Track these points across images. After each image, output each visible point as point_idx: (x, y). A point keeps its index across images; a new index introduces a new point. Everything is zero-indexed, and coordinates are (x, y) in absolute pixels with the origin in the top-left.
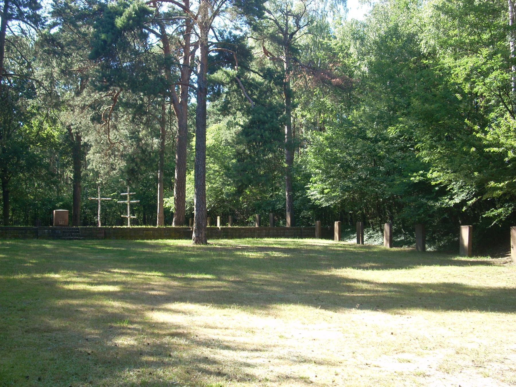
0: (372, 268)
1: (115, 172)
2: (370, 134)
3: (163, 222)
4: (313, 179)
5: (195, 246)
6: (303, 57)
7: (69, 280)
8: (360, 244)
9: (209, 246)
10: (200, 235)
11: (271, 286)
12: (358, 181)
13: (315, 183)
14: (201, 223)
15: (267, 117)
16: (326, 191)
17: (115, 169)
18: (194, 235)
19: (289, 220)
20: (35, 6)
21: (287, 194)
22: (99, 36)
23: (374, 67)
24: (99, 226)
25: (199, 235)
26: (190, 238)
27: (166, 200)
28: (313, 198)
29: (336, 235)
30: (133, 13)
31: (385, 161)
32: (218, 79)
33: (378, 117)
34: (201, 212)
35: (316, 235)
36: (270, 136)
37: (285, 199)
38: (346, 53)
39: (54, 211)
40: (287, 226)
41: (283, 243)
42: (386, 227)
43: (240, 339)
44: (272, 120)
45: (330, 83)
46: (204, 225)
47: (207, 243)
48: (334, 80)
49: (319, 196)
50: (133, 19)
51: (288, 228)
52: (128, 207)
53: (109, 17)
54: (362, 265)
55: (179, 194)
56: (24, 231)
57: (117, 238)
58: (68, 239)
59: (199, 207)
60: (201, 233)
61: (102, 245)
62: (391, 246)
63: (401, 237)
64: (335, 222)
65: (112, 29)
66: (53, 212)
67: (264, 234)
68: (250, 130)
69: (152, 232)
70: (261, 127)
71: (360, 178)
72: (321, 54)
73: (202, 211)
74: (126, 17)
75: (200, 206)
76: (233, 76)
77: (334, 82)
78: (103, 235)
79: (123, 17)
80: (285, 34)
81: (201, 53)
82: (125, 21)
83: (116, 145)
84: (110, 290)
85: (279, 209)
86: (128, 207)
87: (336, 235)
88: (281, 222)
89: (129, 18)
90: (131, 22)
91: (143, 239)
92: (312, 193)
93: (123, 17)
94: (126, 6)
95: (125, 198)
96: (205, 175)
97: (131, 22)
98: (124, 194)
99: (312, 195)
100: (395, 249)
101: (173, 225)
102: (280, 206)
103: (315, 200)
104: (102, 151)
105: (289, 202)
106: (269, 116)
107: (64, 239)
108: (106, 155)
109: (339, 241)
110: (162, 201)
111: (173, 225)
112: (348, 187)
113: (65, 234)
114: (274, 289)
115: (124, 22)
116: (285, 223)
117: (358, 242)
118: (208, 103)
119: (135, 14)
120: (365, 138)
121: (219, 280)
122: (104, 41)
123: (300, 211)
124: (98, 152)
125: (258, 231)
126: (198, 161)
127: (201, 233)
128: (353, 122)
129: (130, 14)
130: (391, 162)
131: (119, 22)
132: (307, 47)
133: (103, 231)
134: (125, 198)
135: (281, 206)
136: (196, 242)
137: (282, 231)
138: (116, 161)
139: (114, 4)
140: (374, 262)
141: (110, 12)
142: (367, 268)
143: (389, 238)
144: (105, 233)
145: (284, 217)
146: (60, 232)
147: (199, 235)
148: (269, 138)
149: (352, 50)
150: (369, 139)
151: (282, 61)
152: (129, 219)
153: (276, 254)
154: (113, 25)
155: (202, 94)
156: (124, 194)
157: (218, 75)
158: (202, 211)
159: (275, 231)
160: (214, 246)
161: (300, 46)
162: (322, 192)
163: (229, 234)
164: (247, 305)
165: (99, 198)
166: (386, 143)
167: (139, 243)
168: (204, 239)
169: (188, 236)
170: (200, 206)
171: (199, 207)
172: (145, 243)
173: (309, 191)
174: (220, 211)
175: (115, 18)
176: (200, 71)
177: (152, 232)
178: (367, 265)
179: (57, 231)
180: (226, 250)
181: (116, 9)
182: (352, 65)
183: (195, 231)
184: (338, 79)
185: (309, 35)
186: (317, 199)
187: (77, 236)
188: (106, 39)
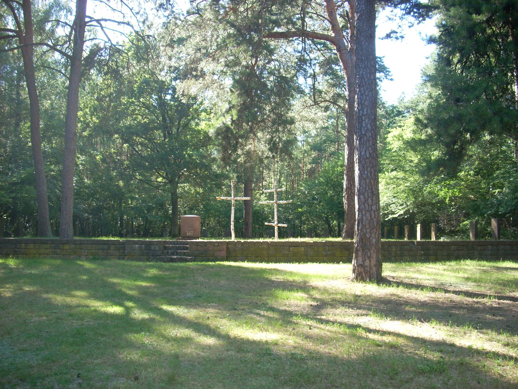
10: (367, 263)
11: (320, 39)
14: (368, 236)
25: (364, 261)
34: (368, 215)
46: (374, 240)
47: (381, 280)
56: (105, 247)
59: (364, 204)
60: (369, 258)
67: (489, 252)
69: (303, 249)
73: (370, 212)
84: (250, 338)
96: (495, 307)
113: (165, 251)
125: (479, 248)
126: (360, 108)
127: (369, 258)
133: (225, 246)
146: (157, 248)
147: (364, 261)
152: (276, 228)
158: (370, 212)
163: (431, 252)
165: (233, 197)
170: (366, 200)
171: (364, 204)
174: (422, 217)
177: (303, 249)
179: (153, 247)
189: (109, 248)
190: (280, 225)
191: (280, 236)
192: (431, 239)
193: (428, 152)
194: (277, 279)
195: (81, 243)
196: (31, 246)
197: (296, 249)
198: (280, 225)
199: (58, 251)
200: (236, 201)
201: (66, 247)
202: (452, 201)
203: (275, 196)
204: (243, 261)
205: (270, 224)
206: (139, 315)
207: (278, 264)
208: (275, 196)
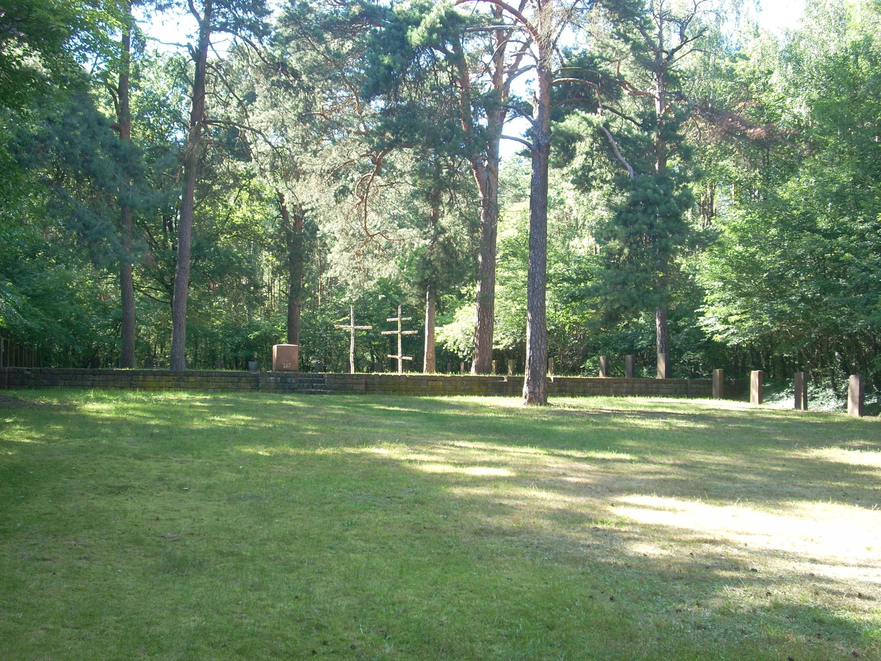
0: (862, 448)
1: (371, 283)
2: (822, 223)
3: (434, 367)
4: (709, 298)
5: (529, 407)
6: (694, 89)
7: (480, 453)
8: (800, 408)
9: (552, 408)
10: (537, 390)
12: (800, 301)
13: (712, 305)
15: (659, 193)
16: (732, 319)
17: (371, 279)
18: (525, 389)
19: (662, 367)
20: (258, 5)
21: (658, 322)
22: (378, 59)
23: (820, 109)
24: (352, 372)
25: (534, 389)
26: (519, 393)
27: (437, 329)
28: (710, 329)
29: (754, 393)
30: (438, 20)
31: (852, 269)
32: (574, 131)
33: (837, 194)
35: (714, 393)
36: (665, 226)
37: (655, 332)
38: (764, 84)
39: (275, 347)
40: (659, 377)
41: (669, 405)
42: (853, 382)
43: (798, 549)
44: (666, 199)
45: (744, 136)
48: (752, 131)
49: (721, 327)
50: (438, 31)
51: (659, 381)
52: (399, 341)
53: (395, 28)
54: (849, 443)
55: (484, 320)
56: (236, 379)
57: (385, 392)
58: (307, 393)
61: (381, 403)
62: (862, 413)
63: (871, 398)
64: (753, 372)
65: (402, 47)
66: (271, 351)
67: (625, 390)
68: (630, 215)
70: (650, 211)
71: (804, 298)
72: (720, 85)
74: (426, 28)
75: (537, 341)
76: (598, 125)
77: (751, 134)
78: (362, 387)
79: (420, 28)
80: (659, 51)
81: (540, 86)
82: (426, 34)
83: (376, 238)
85: (642, 348)
86: (399, 341)
87: (754, 393)
88: (645, 370)
89: (431, 30)
90: (435, 36)
91: (435, 395)
92: (706, 323)
93: (422, 28)
94: (423, 9)
95: (393, 326)
97: (435, 36)
98: (393, 319)
99: (706, 326)
100: (867, 419)
101: (473, 373)
102: (642, 343)
103: (713, 333)
104: (353, 248)
105: (662, 336)
106: (662, 192)
107: (301, 393)
108: (358, 255)
109: (760, 402)
110: (431, 331)
111: (473, 373)
112: (783, 313)
114: (751, 477)
115: (423, 37)
116: (653, 371)
117: (797, 405)
118: (551, 171)
119: (440, 23)
120: (814, 230)
121: (645, 461)
122: (389, 68)
123: (680, 352)
124: (347, 250)
125: (614, 385)
127: (539, 386)
128: (792, 203)
129: (434, 23)
130: (863, 271)
131: (415, 36)
132: (692, 75)
133: (363, 380)
134: (393, 326)
135: (644, 343)
136: (530, 401)
137: (654, 386)
138: (374, 264)
139: (406, 6)
140: (865, 439)
141: (397, 20)
142: (855, 448)
143: (857, 400)
144: (366, 384)
145: (654, 363)
146: (294, 381)
147: (534, 389)
148: (663, 230)
149: (774, 79)
150: (819, 231)
151: (654, 97)
153: (682, 424)
154: (404, 42)
155: (542, 156)
156: (393, 319)
157: (573, 123)
159: (644, 385)
160: (562, 408)
161: (680, 71)
162: (725, 321)
164: (743, 500)
166: (852, 238)
167: (426, 400)
168: (542, 396)
169: (513, 389)
170: (537, 341)
172: (433, 401)
173: (701, 318)
175: (407, 29)
176: (539, 117)
178: (855, 443)
179: (289, 380)
180: (582, 414)
181: (406, 14)
182: (773, 103)
183: (528, 383)
184: (759, 129)
185: (697, 53)
186: (718, 332)
187: (321, 387)
188: (392, 64)
189: (239, 381)
190: (404, 358)
191: (404, 369)
192: (422, 371)
193: (202, 208)
194: (627, 406)
195: (209, 375)
196: (151, 378)
197: (434, 383)
198: (404, 358)
199: (182, 384)
200: (356, 330)
201: (192, 379)
202: (573, 329)
203: (399, 326)
204: (443, 395)
205: (394, 356)
206: (216, 463)
207: (483, 397)
208: (399, 326)
